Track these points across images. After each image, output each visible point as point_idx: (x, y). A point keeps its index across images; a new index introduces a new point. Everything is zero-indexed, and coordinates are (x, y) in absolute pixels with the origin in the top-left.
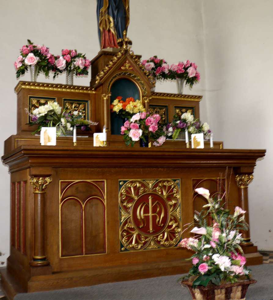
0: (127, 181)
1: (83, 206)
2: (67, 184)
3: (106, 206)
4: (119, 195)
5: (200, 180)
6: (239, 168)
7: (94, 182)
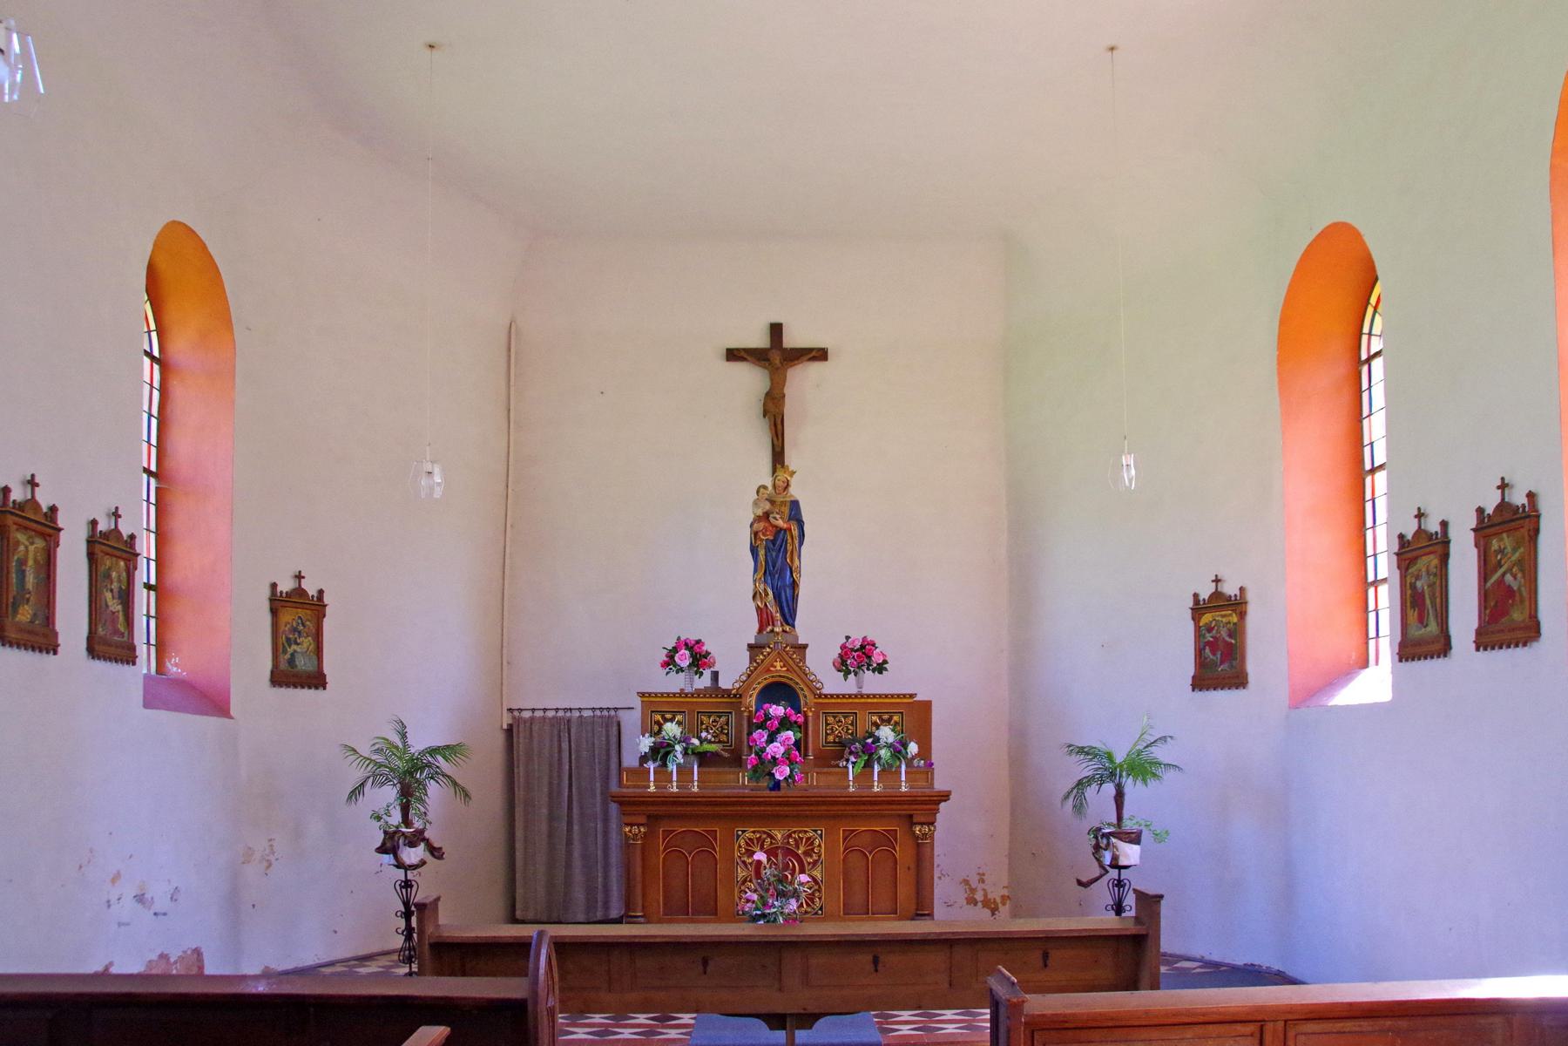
1: (690, 859)
4: (736, 848)
6: (911, 816)
7: (884, 830)
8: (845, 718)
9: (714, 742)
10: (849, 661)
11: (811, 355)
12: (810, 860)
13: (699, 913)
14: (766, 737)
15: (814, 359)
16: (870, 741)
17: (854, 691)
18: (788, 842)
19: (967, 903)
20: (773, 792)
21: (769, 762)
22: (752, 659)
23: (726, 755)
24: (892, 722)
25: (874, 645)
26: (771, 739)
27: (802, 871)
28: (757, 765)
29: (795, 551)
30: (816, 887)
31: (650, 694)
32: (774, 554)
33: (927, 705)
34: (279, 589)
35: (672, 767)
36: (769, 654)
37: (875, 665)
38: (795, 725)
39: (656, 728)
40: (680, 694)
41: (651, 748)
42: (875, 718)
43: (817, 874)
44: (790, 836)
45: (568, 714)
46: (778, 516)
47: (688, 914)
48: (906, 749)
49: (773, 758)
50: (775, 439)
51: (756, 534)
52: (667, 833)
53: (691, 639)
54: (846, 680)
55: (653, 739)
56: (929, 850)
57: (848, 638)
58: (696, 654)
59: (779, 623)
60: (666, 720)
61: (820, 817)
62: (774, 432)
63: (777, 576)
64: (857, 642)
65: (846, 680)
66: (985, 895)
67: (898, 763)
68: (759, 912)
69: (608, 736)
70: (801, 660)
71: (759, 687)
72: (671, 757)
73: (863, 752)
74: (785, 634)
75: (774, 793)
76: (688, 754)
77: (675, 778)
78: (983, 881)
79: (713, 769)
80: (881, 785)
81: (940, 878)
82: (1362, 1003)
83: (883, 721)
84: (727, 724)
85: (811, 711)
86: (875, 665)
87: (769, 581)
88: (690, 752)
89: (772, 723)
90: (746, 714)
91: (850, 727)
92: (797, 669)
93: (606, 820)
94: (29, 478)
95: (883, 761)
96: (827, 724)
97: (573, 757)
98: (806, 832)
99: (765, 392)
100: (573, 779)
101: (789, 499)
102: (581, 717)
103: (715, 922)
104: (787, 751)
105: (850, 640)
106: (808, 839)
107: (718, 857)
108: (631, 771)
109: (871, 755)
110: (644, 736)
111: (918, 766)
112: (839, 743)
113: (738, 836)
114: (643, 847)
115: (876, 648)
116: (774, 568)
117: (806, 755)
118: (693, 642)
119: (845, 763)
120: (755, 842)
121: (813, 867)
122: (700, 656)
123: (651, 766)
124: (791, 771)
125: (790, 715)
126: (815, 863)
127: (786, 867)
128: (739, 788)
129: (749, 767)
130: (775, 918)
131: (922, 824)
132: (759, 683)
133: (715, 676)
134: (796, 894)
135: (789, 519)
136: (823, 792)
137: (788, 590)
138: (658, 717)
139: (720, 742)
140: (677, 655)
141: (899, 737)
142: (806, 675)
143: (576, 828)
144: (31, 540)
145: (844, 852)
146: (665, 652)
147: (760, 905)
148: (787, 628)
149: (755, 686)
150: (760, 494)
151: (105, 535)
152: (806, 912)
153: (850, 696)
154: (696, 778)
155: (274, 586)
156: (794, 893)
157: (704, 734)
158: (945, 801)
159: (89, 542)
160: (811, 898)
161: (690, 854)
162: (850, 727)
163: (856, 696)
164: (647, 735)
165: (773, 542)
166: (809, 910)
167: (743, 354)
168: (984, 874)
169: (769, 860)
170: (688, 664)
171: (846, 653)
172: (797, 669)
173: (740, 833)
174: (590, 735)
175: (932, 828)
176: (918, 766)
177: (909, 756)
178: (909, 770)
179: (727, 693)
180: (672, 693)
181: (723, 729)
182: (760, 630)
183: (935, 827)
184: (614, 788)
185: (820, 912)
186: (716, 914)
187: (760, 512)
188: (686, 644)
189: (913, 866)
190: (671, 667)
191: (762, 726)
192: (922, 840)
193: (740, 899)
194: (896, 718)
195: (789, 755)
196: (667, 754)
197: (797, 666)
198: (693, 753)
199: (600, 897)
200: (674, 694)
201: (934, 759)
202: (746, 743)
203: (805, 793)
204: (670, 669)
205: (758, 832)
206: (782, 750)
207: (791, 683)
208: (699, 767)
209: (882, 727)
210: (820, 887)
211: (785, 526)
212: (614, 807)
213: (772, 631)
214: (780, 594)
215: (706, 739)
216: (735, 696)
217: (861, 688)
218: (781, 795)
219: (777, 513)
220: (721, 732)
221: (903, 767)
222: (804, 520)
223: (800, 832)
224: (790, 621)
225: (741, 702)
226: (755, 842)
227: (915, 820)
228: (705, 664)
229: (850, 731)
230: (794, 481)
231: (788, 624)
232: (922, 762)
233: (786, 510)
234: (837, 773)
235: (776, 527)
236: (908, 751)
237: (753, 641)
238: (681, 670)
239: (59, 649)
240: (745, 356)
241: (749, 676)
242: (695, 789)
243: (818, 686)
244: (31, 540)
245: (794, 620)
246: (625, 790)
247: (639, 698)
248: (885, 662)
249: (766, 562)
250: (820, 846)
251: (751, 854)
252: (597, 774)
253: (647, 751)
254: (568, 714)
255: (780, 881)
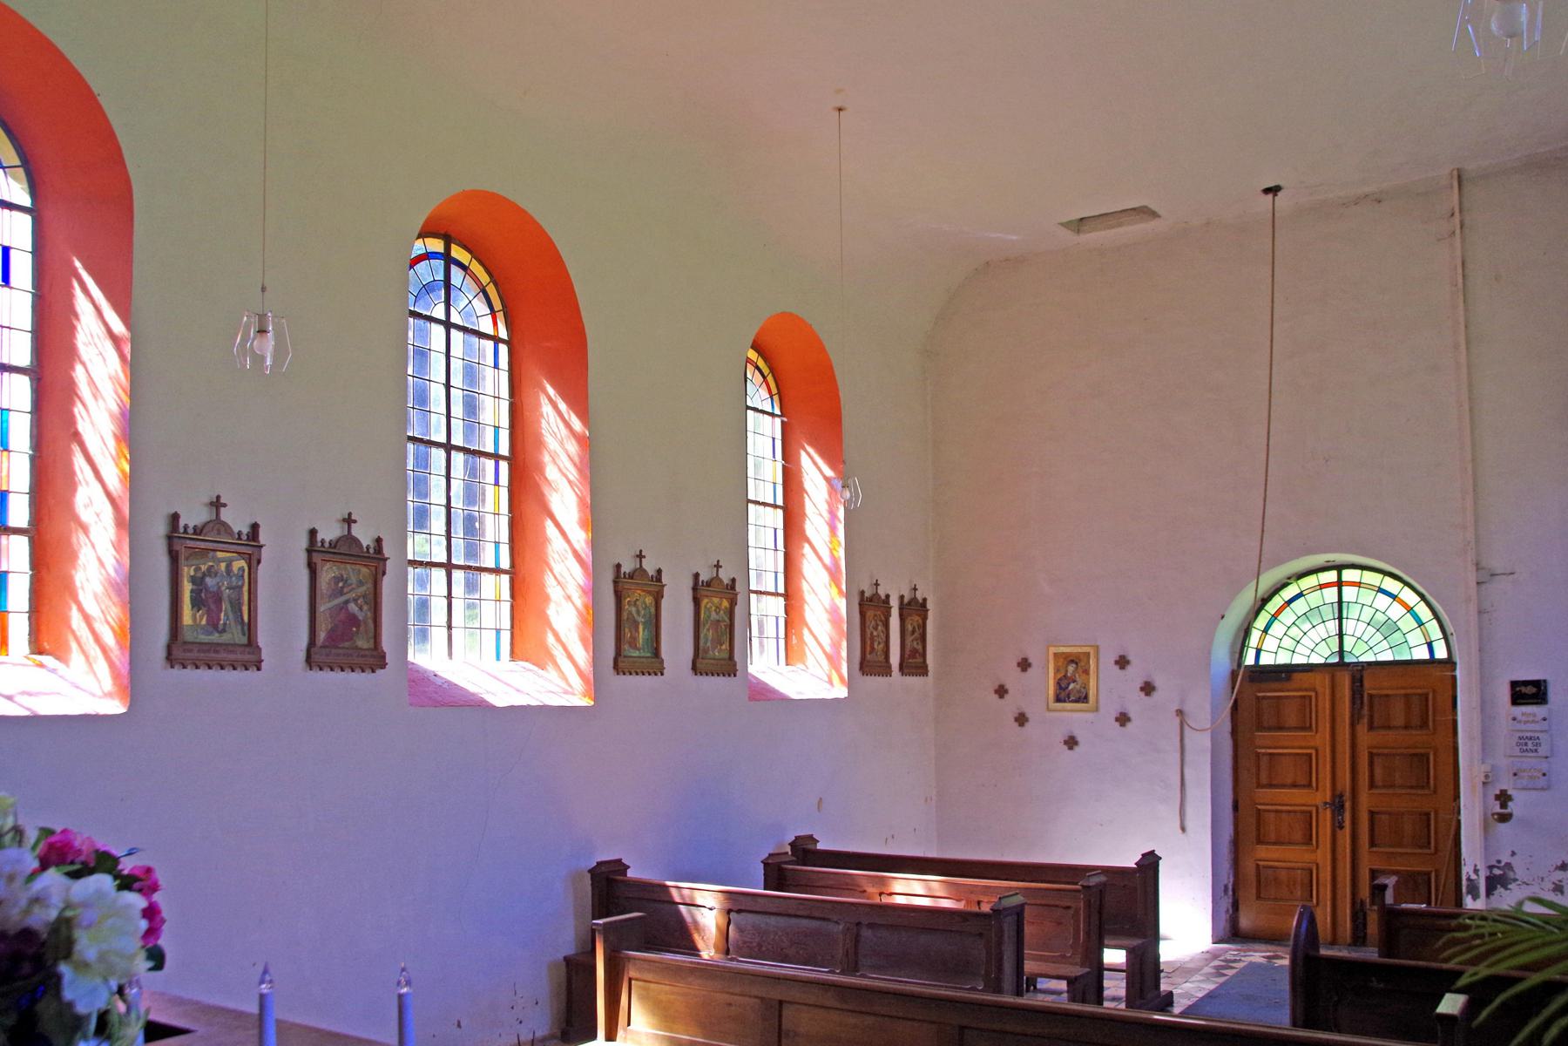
34: (319, 537)
82: (462, 689)
94: (638, 553)
144: (213, 575)
151: (871, 599)
155: (313, 533)
159: (860, 605)
239: (665, 671)
244: (213, 575)
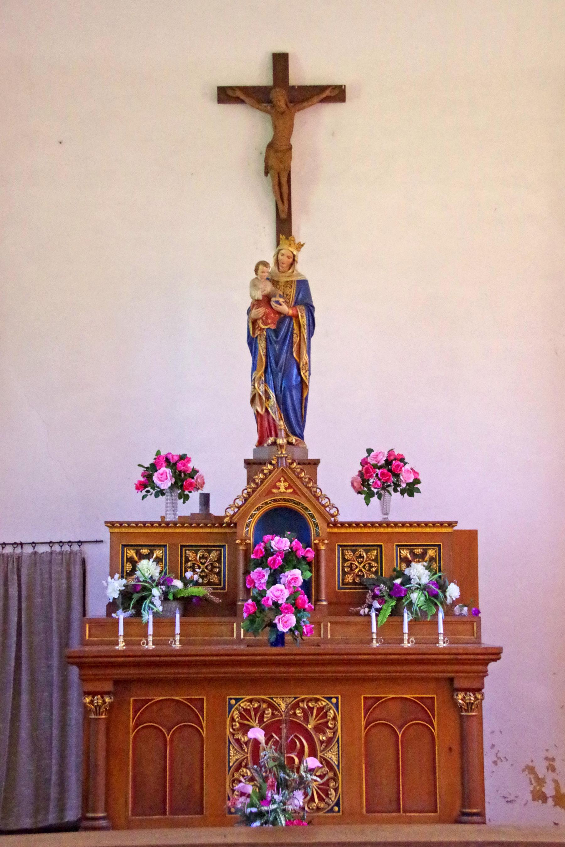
0: (242, 699)
1: (168, 738)
2: (293, 699)
3: (205, 739)
5: (378, 699)
6: (451, 680)
8: (367, 552)
9: (202, 584)
10: (371, 481)
11: (324, 95)
12: (322, 737)
13: (183, 811)
14: (266, 577)
15: (327, 100)
16: (398, 581)
17: (378, 517)
18: (295, 713)
19: (534, 799)
20: (274, 648)
21: (270, 609)
22: (250, 479)
23: (217, 600)
24: (427, 558)
25: (402, 459)
26: (274, 580)
27: (313, 754)
28: (255, 613)
29: (302, 344)
30: (331, 774)
31: (121, 524)
32: (277, 347)
33: (472, 535)
35: (147, 617)
36: (270, 472)
37: (404, 485)
38: (303, 562)
39: (128, 567)
40: (160, 524)
41: (122, 593)
42: (405, 553)
43: (332, 756)
44: (296, 706)
45: (18, 550)
46: (281, 300)
47: (164, 813)
48: (444, 592)
49: (276, 604)
50: (280, 204)
51: (254, 322)
52: (139, 704)
53: (173, 453)
54: (367, 505)
55: (124, 581)
56: (475, 725)
57: (369, 451)
58: (180, 472)
59: (283, 433)
60: (142, 557)
61: (336, 680)
62: (278, 193)
63: (280, 375)
64: (380, 457)
65: (367, 505)
66: (557, 788)
67: (434, 610)
68: (254, 810)
69: (69, 578)
70: (310, 480)
71: (259, 514)
72: (147, 602)
73: (390, 596)
74: (290, 447)
75: (275, 650)
76: (169, 600)
77: (150, 631)
78: (553, 769)
79: (200, 619)
80: (412, 639)
81: (495, 763)
83: (414, 555)
84: (219, 560)
85: (324, 543)
86: (404, 485)
87: (271, 382)
88: (171, 597)
89: (274, 560)
90: (241, 548)
91: (373, 564)
92: (305, 490)
93: (64, 687)
95: (415, 608)
96: (344, 560)
97: (24, 605)
98: (317, 700)
99: (268, 143)
100: (23, 635)
101: (295, 279)
102: (35, 553)
103: (200, 825)
104: (293, 594)
105: (372, 454)
106: (320, 709)
107: (204, 735)
108: (96, 623)
109: (399, 599)
110: (112, 577)
111: (461, 614)
112: (360, 584)
113: (231, 707)
114: (108, 722)
115: (405, 464)
116: (277, 365)
117: (318, 600)
118: (176, 458)
119: (367, 610)
120: (253, 713)
121: (326, 747)
122: (185, 475)
123: (121, 616)
124: (298, 620)
125: (297, 550)
126: (330, 741)
127: (292, 747)
128: (233, 643)
129: (245, 615)
130: (275, 817)
131: (466, 690)
132: (258, 509)
133: (205, 499)
134: (302, 784)
135: (297, 303)
136: (342, 647)
137: (295, 393)
138: (132, 553)
139: (209, 584)
140: (156, 474)
141: (436, 576)
142: (318, 498)
143: (25, 698)
145: (365, 728)
146: (142, 470)
147: (256, 800)
148: (293, 439)
149: (252, 512)
150: (259, 272)
152: (318, 809)
153: (373, 524)
154: (178, 630)
156: (300, 784)
157: (189, 574)
158: (495, 660)
160: (324, 790)
161: (169, 731)
162: (373, 564)
163: (380, 525)
164: (117, 576)
165: (276, 332)
166: (322, 805)
167: (239, 94)
168: (553, 759)
169: (268, 738)
170: (169, 484)
171: (367, 471)
172: (305, 490)
173: (233, 702)
174: (46, 576)
175: (479, 696)
176: (461, 614)
177: (449, 601)
178: (449, 619)
179: (219, 521)
180: (142, 522)
181: (213, 567)
182: (260, 443)
183: (483, 695)
184: (76, 647)
185: (336, 809)
186: (201, 812)
187: (259, 295)
188: (167, 461)
189: (456, 747)
190: (149, 489)
191: (261, 563)
192: (466, 711)
193: (233, 791)
194: (431, 553)
195: (295, 600)
196: (143, 598)
197: (298, 478)
198: (175, 598)
199: (54, 793)
200: (152, 524)
201: (482, 605)
202: (241, 586)
203: (313, 649)
204: (148, 492)
205: (258, 701)
206: (287, 593)
207: (305, 514)
208: (183, 615)
209: (413, 564)
210: (335, 774)
211: (291, 312)
212: (74, 671)
213: (274, 443)
214: (284, 397)
215: (191, 581)
216: (228, 525)
217: (387, 514)
218: (286, 652)
219: (280, 296)
220: (211, 571)
221: (441, 615)
222: (315, 304)
223: (310, 700)
224: (298, 430)
225: (235, 533)
226: (253, 713)
227: (457, 684)
228: (191, 485)
229: (374, 569)
230: (301, 256)
231: (295, 434)
232: (466, 609)
233: (292, 292)
234: (356, 624)
235: (279, 313)
236: (447, 594)
237: (251, 456)
238: (161, 493)
240: (242, 97)
241: (246, 500)
242: (177, 646)
243: (324, 502)
245: (302, 427)
246: (87, 648)
247: (107, 529)
248: (417, 481)
249: (267, 356)
250: (335, 718)
251: (245, 729)
252: (55, 626)
253: (116, 596)
254: (18, 550)
255: (281, 767)
